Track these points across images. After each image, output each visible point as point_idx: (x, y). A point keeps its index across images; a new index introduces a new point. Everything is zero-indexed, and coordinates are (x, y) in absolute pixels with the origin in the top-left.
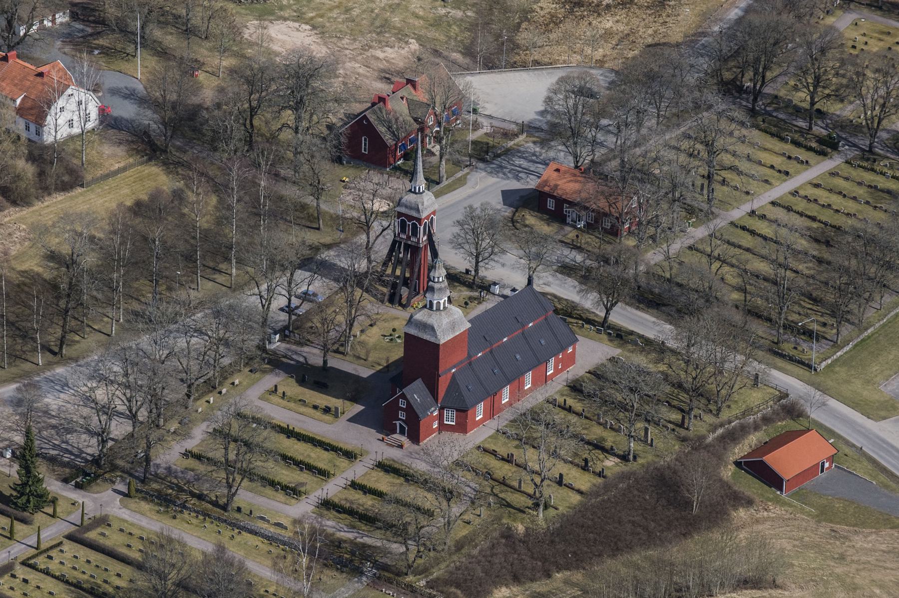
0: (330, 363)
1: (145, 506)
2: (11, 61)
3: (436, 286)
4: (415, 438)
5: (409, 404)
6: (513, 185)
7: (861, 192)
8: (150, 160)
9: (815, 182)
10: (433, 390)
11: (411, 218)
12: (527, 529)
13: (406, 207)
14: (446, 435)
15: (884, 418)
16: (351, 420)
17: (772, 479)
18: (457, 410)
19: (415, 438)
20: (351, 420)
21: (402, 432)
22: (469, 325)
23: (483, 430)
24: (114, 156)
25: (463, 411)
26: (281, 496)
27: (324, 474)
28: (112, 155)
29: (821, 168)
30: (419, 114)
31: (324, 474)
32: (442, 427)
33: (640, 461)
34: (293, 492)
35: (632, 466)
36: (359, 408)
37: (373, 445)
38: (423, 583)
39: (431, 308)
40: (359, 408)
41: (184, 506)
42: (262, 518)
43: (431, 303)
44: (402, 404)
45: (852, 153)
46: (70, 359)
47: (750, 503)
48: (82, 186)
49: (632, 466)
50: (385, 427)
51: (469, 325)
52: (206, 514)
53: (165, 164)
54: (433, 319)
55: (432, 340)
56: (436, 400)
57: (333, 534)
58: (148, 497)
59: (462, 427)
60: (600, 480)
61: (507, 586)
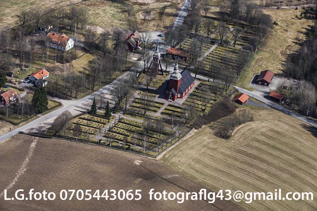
0: (148, 88)
1: (129, 116)
2: (55, 35)
3: (177, 69)
4: (173, 100)
5: (172, 93)
6: (161, 54)
7: (224, 51)
8: (87, 53)
9: (215, 49)
10: (176, 90)
11: (156, 58)
12: (203, 115)
13: (155, 56)
14: (179, 99)
15: (253, 91)
16: (158, 97)
17: (240, 103)
18: (181, 94)
19: (173, 100)
20: (158, 97)
21: (170, 99)
22: (169, 79)
23: (185, 97)
24: (79, 52)
25: (182, 94)
26: (153, 112)
27: (159, 108)
28: (80, 53)
29: (214, 47)
30: (137, 41)
31: (159, 108)
32: (178, 97)
33: (218, 101)
34: (155, 111)
35: (216, 102)
36: (158, 95)
37: (166, 102)
38: (189, 125)
39: (175, 73)
40: (158, 95)
41: (136, 115)
42: (152, 116)
43: (175, 72)
44: (171, 93)
45: (218, 44)
46: (95, 91)
47: (238, 108)
48: (78, 58)
49: (216, 102)
50: (167, 98)
51: (169, 79)
52: (141, 117)
53: (90, 53)
54: (176, 75)
55: (176, 79)
56: (177, 92)
57: (167, 118)
58: (127, 114)
59: (181, 97)
60: (212, 105)
61: (204, 125)
